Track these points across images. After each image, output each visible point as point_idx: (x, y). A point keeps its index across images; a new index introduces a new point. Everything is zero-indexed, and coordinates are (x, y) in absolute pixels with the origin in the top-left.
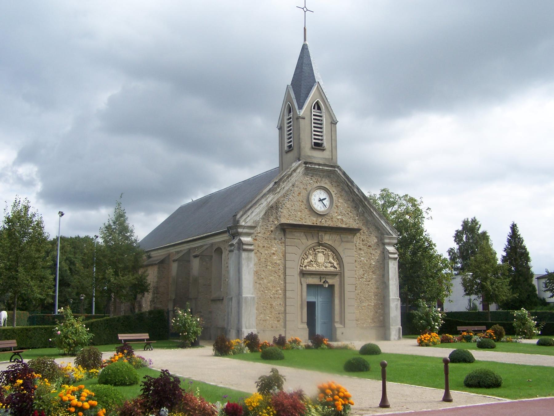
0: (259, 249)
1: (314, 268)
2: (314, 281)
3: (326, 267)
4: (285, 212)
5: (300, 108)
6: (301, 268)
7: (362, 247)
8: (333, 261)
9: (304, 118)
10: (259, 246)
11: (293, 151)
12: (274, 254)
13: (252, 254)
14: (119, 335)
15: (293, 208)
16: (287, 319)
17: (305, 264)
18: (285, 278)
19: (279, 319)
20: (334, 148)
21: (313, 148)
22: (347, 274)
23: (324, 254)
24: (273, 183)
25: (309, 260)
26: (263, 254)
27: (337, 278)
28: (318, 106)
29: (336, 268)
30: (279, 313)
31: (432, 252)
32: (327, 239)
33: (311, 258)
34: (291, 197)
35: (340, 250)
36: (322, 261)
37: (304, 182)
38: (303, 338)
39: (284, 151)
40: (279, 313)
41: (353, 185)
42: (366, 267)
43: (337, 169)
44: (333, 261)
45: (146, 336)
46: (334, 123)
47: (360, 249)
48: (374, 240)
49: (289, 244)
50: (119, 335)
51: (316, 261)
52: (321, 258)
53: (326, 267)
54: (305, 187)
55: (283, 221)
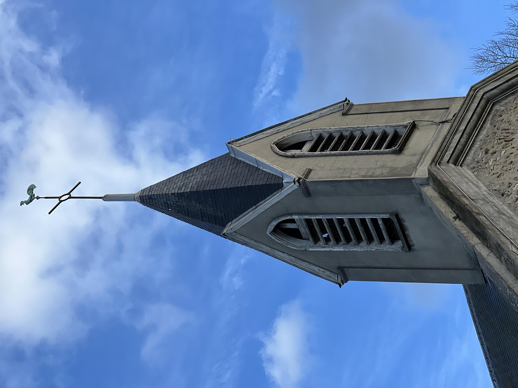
5: (275, 184)
9: (310, 171)
11: (403, 216)
20: (419, 106)
21: (400, 151)
24: (458, 223)
28: (283, 146)
37: (498, 169)
39: (407, 258)
46: (347, 108)
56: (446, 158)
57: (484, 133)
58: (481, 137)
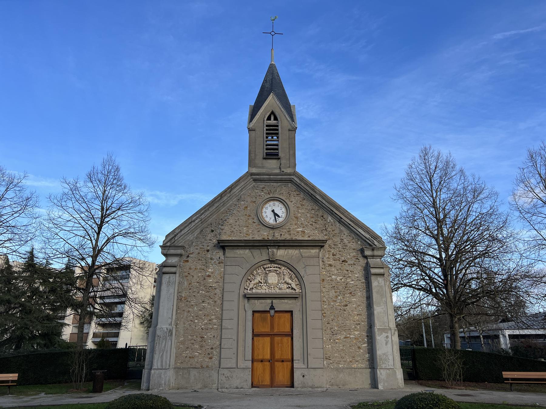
0: (191, 271)
1: (264, 290)
2: (260, 305)
3: (280, 289)
4: (226, 228)
6: (246, 291)
7: (332, 262)
8: (290, 281)
10: (190, 269)
12: (209, 276)
13: (177, 278)
14: (503, 373)
15: (237, 224)
16: (222, 357)
17: (251, 286)
18: (222, 304)
19: (211, 355)
21: (264, 159)
22: (310, 296)
23: (277, 274)
25: (256, 281)
26: (195, 277)
27: (298, 302)
29: (295, 290)
30: (212, 348)
31: (498, 279)
32: (281, 253)
33: (258, 279)
34: (235, 212)
35: (300, 268)
36: (275, 281)
38: (267, 381)
40: (212, 348)
41: (315, 192)
42: (341, 288)
43: (292, 177)
44: (290, 281)
45: (14, 376)
47: (330, 265)
48: (350, 254)
49: (228, 264)
50: (503, 373)
51: (266, 282)
52: (273, 278)
53: (280, 289)
54: (254, 199)
55: (224, 238)
56: (254, 177)
57: (275, 184)
58: (272, 184)
